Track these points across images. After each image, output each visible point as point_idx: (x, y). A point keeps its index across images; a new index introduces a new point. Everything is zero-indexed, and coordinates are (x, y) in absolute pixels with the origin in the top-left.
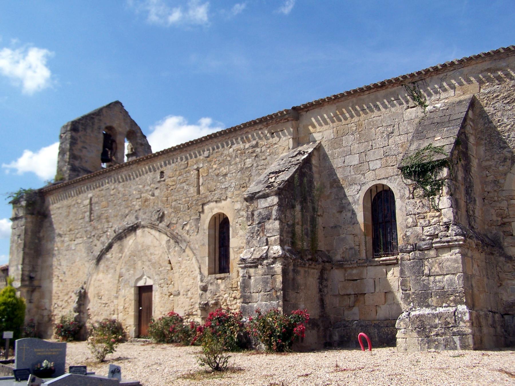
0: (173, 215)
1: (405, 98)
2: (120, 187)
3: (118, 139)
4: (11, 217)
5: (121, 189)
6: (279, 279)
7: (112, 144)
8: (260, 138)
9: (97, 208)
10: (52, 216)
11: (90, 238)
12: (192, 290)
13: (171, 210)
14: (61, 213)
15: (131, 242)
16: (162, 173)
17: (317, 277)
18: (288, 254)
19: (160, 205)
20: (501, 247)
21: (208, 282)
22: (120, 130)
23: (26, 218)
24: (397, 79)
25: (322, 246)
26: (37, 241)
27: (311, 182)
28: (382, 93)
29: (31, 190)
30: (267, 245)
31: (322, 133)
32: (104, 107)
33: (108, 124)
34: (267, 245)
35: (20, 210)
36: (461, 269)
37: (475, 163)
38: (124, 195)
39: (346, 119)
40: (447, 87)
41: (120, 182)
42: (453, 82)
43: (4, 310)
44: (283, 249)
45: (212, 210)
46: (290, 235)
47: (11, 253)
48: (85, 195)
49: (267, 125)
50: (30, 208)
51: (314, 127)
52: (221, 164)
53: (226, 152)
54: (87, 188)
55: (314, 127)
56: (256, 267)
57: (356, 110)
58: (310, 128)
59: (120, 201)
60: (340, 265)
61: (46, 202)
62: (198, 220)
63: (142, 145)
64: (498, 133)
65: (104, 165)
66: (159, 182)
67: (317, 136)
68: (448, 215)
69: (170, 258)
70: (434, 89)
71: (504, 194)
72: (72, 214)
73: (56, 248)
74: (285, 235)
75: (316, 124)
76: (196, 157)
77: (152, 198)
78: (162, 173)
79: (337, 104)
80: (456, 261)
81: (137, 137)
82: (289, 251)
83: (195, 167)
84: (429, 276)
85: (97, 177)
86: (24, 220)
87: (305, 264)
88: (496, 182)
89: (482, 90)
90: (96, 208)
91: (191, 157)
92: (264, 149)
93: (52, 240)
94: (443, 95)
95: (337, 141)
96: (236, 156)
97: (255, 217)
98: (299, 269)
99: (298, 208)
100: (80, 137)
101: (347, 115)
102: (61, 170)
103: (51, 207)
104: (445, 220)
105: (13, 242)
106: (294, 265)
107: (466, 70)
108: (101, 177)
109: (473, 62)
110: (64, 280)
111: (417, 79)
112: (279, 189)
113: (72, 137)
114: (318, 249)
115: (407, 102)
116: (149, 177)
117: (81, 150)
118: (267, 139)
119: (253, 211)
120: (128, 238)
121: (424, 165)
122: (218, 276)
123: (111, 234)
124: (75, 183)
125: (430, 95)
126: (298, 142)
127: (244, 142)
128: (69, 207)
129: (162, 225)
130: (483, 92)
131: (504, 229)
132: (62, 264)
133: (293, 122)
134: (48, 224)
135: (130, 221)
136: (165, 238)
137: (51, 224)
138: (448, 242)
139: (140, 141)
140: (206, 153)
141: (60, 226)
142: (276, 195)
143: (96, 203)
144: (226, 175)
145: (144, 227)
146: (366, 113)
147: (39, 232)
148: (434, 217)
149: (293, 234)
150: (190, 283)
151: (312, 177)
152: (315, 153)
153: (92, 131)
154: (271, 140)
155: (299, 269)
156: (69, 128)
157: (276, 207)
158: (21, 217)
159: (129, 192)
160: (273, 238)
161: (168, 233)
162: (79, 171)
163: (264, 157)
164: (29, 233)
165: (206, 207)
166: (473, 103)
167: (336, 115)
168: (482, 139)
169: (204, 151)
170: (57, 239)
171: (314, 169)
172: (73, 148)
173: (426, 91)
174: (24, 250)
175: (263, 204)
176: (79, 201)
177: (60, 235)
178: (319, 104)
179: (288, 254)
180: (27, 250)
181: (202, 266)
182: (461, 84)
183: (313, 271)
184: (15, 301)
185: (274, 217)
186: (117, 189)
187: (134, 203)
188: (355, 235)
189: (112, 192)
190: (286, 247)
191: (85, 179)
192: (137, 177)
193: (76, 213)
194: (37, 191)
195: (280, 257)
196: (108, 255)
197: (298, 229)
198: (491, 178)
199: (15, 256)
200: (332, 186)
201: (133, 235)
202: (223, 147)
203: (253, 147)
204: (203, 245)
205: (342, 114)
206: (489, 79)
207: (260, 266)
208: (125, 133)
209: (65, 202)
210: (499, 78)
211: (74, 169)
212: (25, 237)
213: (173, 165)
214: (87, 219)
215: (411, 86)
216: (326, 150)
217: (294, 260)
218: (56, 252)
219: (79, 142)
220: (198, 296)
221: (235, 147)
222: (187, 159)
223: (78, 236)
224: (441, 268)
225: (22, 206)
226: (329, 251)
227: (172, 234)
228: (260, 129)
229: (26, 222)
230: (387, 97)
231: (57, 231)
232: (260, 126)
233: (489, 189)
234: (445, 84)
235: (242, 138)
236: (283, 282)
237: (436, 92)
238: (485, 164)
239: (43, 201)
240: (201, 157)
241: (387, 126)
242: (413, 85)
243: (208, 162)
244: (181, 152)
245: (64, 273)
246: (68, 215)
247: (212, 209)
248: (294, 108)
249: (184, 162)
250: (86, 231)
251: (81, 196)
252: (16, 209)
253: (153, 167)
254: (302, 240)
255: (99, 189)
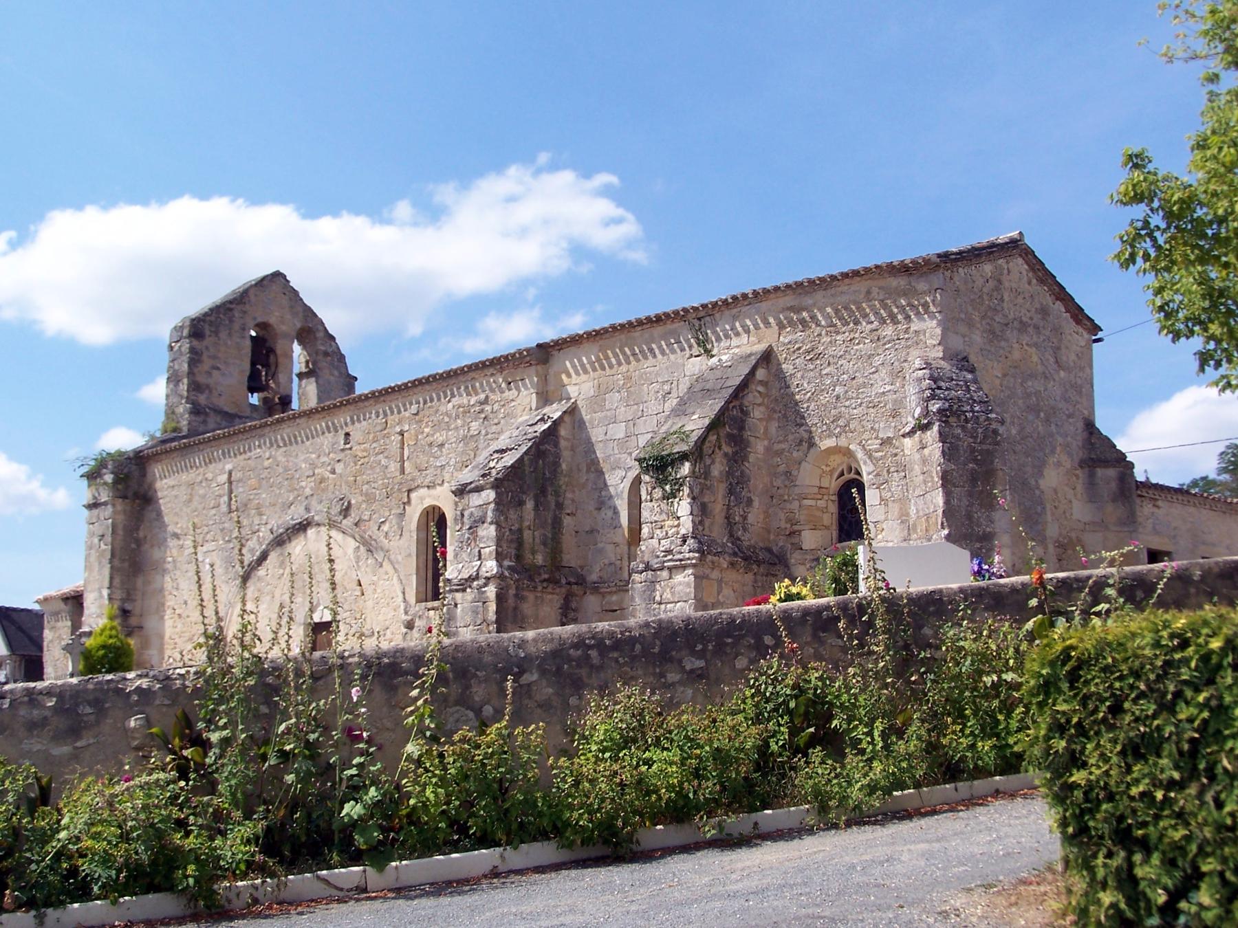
0: (364, 506)
1: (688, 341)
2: (279, 455)
3: (280, 347)
4: (85, 503)
5: (281, 459)
6: (492, 607)
7: (268, 356)
8: (492, 390)
9: (241, 490)
10: (161, 501)
11: (229, 541)
12: (392, 628)
13: (360, 499)
14: (176, 497)
15: (299, 548)
16: (347, 434)
17: (559, 605)
18: (507, 573)
19: (345, 489)
20: (787, 566)
21: (415, 615)
22: (284, 328)
23: (114, 505)
24: (676, 313)
25: (570, 558)
26: (133, 546)
27: (556, 464)
28: (658, 330)
29: (120, 453)
30: (480, 559)
31: (579, 385)
32: (251, 286)
33: (260, 320)
34: (480, 559)
35: (101, 489)
36: (693, 596)
37: (758, 448)
38: (286, 469)
39: (611, 367)
40: (740, 329)
41: (279, 446)
42: (748, 322)
43: (105, 656)
44: (500, 565)
45: (422, 500)
46: (514, 545)
47: (88, 567)
48: (220, 465)
49: (502, 370)
50: (120, 487)
51: (569, 376)
52: (436, 427)
53: (443, 409)
54: (224, 453)
55: (569, 376)
56: (464, 590)
57: (624, 354)
58: (564, 377)
59: (280, 479)
60: (595, 589)
61: (149, 478)
62: (402, 515)
63: (326, 354)
64: (797, 404)
65: (255, 399)
66: (343, 450)
67: (573, 391)
68: (686, 525)
69: (360, 577)
70: (724, 330)
71: (797, 490)
72: (196, 498)
73: (170, 559)
74: (505, 546)
75: (571, 371)
76: (399, 412)
77: (331, 476)
78: (347, 434)
79: (601, 342)
80: (688, 585)
81: (316, 339)
82: (509, 568)
83: (398, 429)
84: (660, 603)
85: (241, 436)
86: (110, 509)
87: (535, 587)
88: (788, 474)
89: (782, 339)
90: (239, 490)
91: (392, 413)
92: (496, 407)
93: (162, 543)
94: (735, 341)
95: (598, 400)
96: (457, 416)
97: (465, 520)
98: (526, 593)
99: (530, 505)
100: (207, 348)
101: (613, 360)
102: (173, 413)
103: (159, 485)
104: (683, 531)
105: (90, 547)
106: (517, 588)
107: (764, 306)
108: (247, 435)
109: (772, 296)
110: (184, 615)
111: (702, 314)
112: (496, 479)
113: (192, 350)
114: (564, 564)
115: (691, 347)
116: (326, 441)
117: (209, 374)
118: (502, 392)
119: (463, 510)
120: (293, 543)
121: (662, 457)
122: (430, 604)
123: (265, 535)
124: (200, 443)
125: (719, 339)
126: (545, 398)
127: (468, 394)
128: (192, 485)
129: (348, 523)
130: (783, 340)
131: (793, 541)
132: (181, 587)
133: (539, 367)
134: (154, 515)
135: (296, 514)
136: (352, 544)
137: (159, 514)
138: (681, 560)
139: (323, 348)
140: (414, 408)
141: (176, 519)
142: (492, 488)
143: (239, 481)
144: (442, 445)
145: (319, 525)
146: (638, 360)
147: (138, 529)
148: (672, 527)
149: (520, 543)
150: (390, 616)
151: (558, 456)
152: (567, 418)
153: (230, 334)
154: (507, 393)
155: (526, 593)
156: (186, 332)
157: (492, 505)
158: (105, 504)
159: (294, 465)
160: (487, 550)
161: (357, 537)
162: (207, 414)
163: (496, 421)
164: (121, 532)
165: (413, 495)
166: (767, 357)
167: (598, 360)
168: (775, 411)
169: (411, 404)
170: (172, 543)
171: (563, 443)
172: (196, 370)
173: (715, 332)
174: (111, 562)
175: (476, 500)
176: (210, 476)
177: (176, 536)
178: (574, 341)
179: (507, 573)
180: (117, 562)
181: (407, 590)
182: (757, 327)
183: (550, 597)
184: (118, 644)
185: (489, 520)
186: (275, 458)
187: (303, 484)
188: (616, 544)
189: (266, 463)
190: (506, 563)
191: (219, 438)
192: (308, 439)
193: (204, 497)
194: (131, 455)
195: (494, 577)
196: (261, 572)
197: (527, 534)
198: (782, 468)
199: (95, 573)
200: (588, 470)
201: (302, 537)
202: (439, 400)
203: (481, 403)
204: (410, 555)
205: (607, 358)
206: (791, 323)
207: (469, 590)
208: (294, 334)
209: (184, 477)
210: (803, 322)
211: (196, 410)
212: (113, 539)
213: (364, 423)
214: (224, 508)
215: (697, 323)
216: (584, 413)
217: (517, 580)
218: (169, 566)
219: (205, 357)
220: (401, 637)
221: (455, 401)
222: (385, 415)
223: (209, 537)
224: (673, 593)
225: (105, 483)
226: (582, 568)
227: (362, 537)
228: (492, 375)
229: (114, 512)
230: (665, 337)
231: (170, 529)
232: (491, 370)
233: (778, 483)
234: (737, 324)
235: (467, 388)
236: (497, 612)
237: (727, 337)
238: (777, 447)
239: (143, 474)
240: (407, 414)
241: (664, 383)
242: (699, 322)
243: (417, 422)
244: (376, 402)
245: (186, 603)
246: (190, 501)
247: (422, 499)
248: (539, 346)
249: (381, 420)
250: (222, 530)
251: (211, 467)
252: (93, 488)
253: (333, 424)
254: (533, 553)
255: (243, 456)
